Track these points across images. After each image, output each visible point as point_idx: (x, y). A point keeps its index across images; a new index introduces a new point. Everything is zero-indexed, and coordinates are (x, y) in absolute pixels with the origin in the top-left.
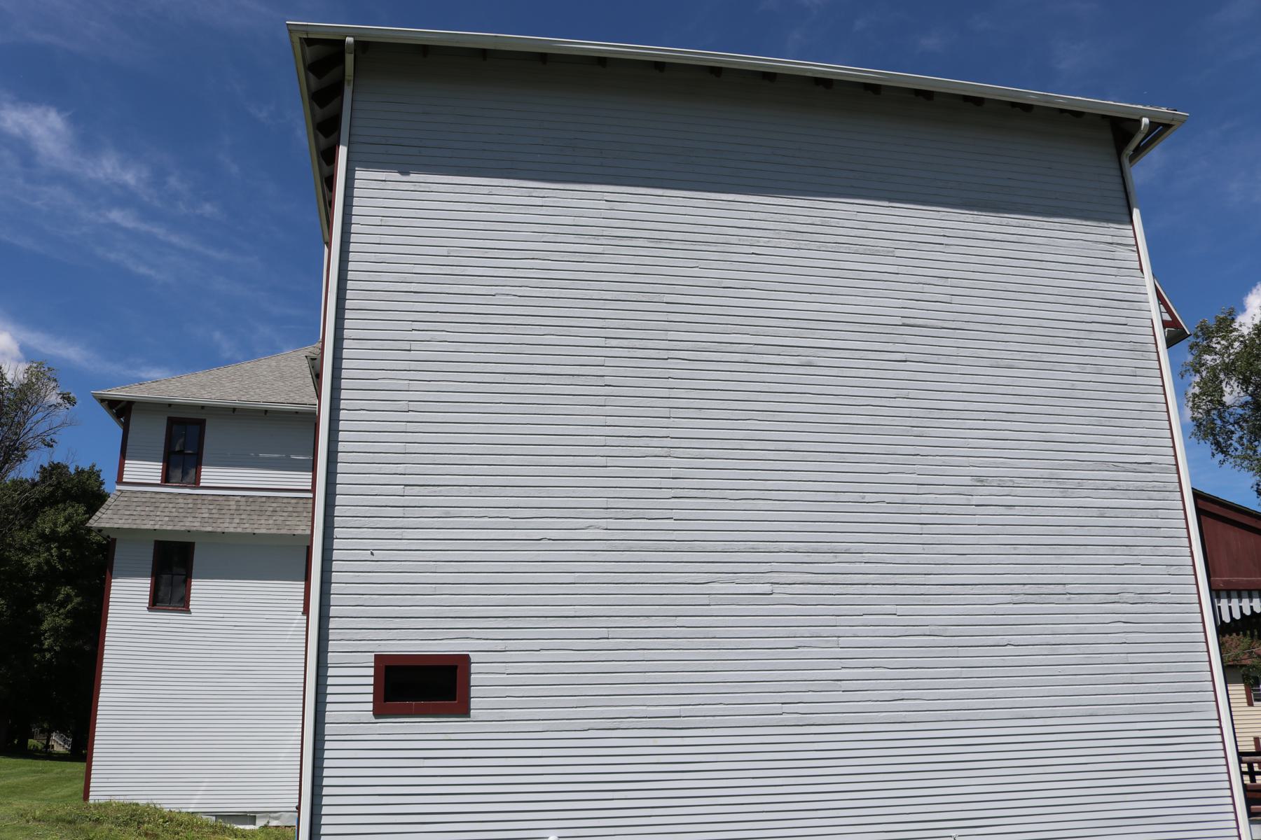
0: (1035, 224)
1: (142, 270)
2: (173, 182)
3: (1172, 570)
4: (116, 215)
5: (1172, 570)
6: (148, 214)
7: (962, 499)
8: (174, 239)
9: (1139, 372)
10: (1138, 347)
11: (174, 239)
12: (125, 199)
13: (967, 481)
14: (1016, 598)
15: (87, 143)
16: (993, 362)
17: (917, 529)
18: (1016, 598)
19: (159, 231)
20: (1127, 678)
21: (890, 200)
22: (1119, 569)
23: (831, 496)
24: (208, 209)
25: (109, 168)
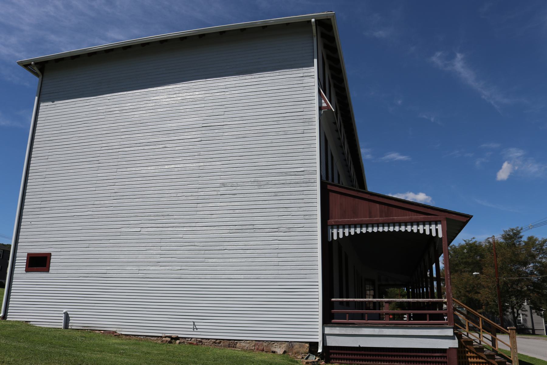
5: (307, 217)
9: (305, 131)
13: (218, 185)
18: (231, 231)
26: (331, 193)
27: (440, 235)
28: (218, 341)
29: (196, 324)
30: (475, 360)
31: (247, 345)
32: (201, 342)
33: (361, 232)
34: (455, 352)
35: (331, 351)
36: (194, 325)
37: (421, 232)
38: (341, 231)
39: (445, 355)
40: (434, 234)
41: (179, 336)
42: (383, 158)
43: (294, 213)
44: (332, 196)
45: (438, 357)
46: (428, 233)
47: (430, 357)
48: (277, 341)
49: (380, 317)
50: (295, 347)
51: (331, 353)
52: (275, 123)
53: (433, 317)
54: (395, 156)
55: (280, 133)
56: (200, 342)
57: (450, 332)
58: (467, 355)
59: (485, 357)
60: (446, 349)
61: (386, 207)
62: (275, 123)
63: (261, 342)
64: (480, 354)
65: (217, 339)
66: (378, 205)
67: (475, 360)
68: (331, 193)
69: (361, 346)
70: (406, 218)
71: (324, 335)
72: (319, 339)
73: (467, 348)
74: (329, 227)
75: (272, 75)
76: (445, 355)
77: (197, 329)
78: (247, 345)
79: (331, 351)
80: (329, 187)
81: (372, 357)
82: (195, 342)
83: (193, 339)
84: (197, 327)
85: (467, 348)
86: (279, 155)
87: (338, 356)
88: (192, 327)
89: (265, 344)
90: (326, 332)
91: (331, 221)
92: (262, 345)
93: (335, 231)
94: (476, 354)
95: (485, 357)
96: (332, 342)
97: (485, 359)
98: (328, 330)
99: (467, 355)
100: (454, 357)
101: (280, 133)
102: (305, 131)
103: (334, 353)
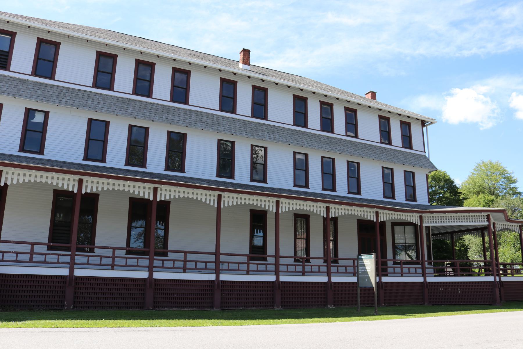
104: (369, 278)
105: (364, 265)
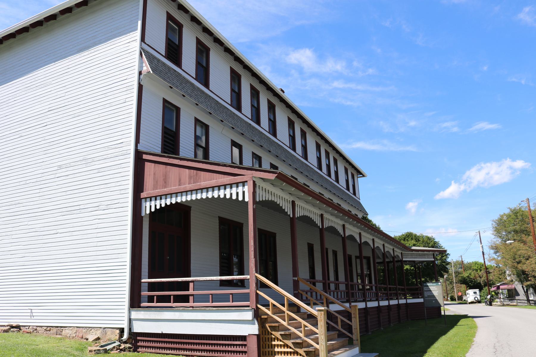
0: (101, 48)
1: (349, 103)
2: (355, 64)
3: (122, 192)
4: (336, 84)
5: (122, 192)
6: (348, 80)
7: (53, 176)
8: (359, 87)
9: (127, 100)
10: (129, 88)
11: (359, 87)
12: (338, 76)
13: (56, 168)
14: (63, 214)
15: (321, 58)
16: (73, 116)
17: (38, 191)
18: (63, 214)
19: (352, 86)
20: (95, 244)
21: (55, 62)
22: (101, 195)
23: (18, 184)
24: (371, 71)
25: (333, 66)
26: (146, 163)
27: (247, 199)
28: (49, 329)
29: (33, 311)
30: (283, 350)
31: (70, 332)
32: (36, 330)
33: (171, 203)
34: (255, 339)
35: (138, 338)
36: (32, 312)
37: (228, 196)
38: (153, 203)
39: (245, 343)
40: (234, 197)
41: (21, 324)
42: (471, 129)
43: (112, 189)
44: (149, 168)
45: (239, 345)
46: (228, 196)
47: (231, 345)
48: (93, 328)
49: (185, 299)
50: (108, 334)
51: (139, 340)
52: (104, 96)
53: (236, 298)
54: (484, 126)
55: (107, 106)
56: (36, 330)
57: (249, 315)
58: (273, 343)
59: (292, 346)
60: (246, 336)
61: (195, 171)
62: (104, 96)
63: (81, 329)
64: (287, 342)
65: (48, 327)
66: (187, 170)
67: (283, 350)
68: (146, 163)
69: (164, 333)
70: (213, 183)
71: (130, 320)
72: (125, 326)
73: (274, 335)
74: (143, 200)
75: (105, 46)
76: (245, 343)
77: (33, 316)
78: (70, 332)
79: (138, 338)
80: (145, 157)
81: (182, 345)
82: (32, 330)
83: (30, 327)
84: (34, 314)
85: (274, 335)
86: (104, 129)
87: (195, 346)
88: (29, 314)
89: (84, 331)
90: (132, 317)
91: (143, 195)
92: (82, 331)
93: (148, 204)
94: (283, 342)
95: (292, 346)
96: (138, 328)
97: (292, 349)
98: (135, 314)
99: (273, 343)
100: (253, 345)
101: (107, 106)
102: (127, 100)
103: (141, 340)
104: (436, 300)
105: (430, 291)
